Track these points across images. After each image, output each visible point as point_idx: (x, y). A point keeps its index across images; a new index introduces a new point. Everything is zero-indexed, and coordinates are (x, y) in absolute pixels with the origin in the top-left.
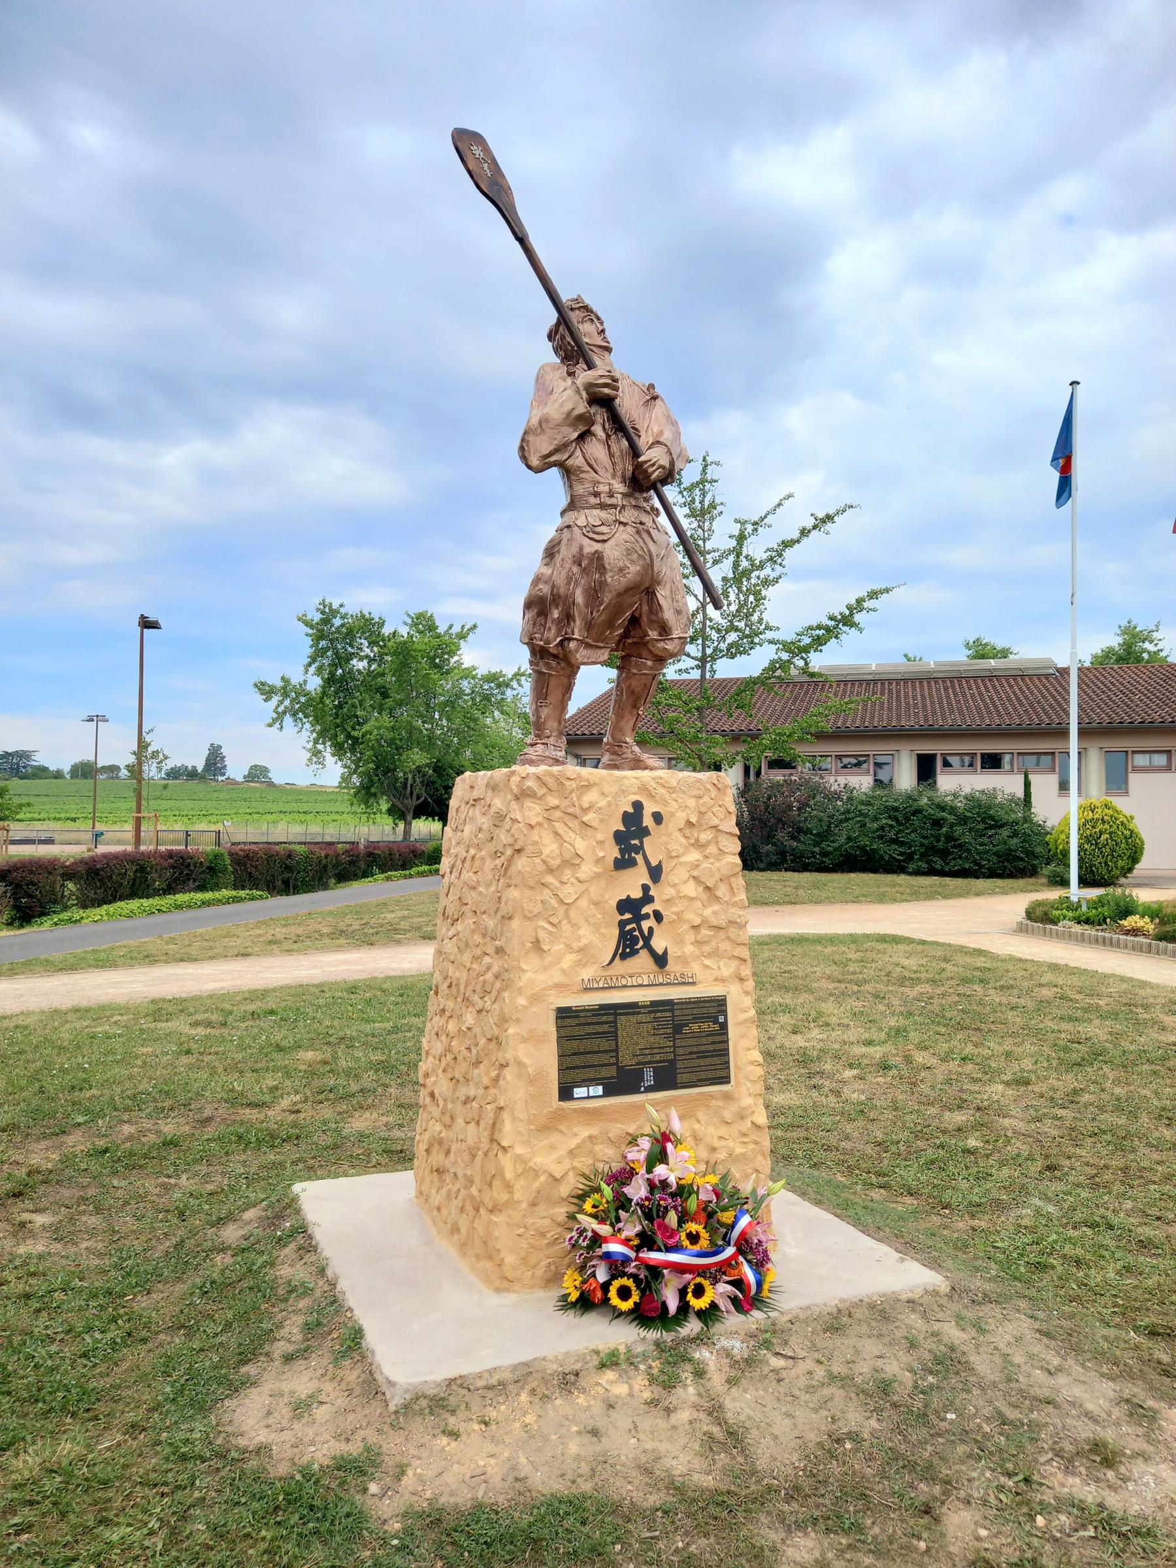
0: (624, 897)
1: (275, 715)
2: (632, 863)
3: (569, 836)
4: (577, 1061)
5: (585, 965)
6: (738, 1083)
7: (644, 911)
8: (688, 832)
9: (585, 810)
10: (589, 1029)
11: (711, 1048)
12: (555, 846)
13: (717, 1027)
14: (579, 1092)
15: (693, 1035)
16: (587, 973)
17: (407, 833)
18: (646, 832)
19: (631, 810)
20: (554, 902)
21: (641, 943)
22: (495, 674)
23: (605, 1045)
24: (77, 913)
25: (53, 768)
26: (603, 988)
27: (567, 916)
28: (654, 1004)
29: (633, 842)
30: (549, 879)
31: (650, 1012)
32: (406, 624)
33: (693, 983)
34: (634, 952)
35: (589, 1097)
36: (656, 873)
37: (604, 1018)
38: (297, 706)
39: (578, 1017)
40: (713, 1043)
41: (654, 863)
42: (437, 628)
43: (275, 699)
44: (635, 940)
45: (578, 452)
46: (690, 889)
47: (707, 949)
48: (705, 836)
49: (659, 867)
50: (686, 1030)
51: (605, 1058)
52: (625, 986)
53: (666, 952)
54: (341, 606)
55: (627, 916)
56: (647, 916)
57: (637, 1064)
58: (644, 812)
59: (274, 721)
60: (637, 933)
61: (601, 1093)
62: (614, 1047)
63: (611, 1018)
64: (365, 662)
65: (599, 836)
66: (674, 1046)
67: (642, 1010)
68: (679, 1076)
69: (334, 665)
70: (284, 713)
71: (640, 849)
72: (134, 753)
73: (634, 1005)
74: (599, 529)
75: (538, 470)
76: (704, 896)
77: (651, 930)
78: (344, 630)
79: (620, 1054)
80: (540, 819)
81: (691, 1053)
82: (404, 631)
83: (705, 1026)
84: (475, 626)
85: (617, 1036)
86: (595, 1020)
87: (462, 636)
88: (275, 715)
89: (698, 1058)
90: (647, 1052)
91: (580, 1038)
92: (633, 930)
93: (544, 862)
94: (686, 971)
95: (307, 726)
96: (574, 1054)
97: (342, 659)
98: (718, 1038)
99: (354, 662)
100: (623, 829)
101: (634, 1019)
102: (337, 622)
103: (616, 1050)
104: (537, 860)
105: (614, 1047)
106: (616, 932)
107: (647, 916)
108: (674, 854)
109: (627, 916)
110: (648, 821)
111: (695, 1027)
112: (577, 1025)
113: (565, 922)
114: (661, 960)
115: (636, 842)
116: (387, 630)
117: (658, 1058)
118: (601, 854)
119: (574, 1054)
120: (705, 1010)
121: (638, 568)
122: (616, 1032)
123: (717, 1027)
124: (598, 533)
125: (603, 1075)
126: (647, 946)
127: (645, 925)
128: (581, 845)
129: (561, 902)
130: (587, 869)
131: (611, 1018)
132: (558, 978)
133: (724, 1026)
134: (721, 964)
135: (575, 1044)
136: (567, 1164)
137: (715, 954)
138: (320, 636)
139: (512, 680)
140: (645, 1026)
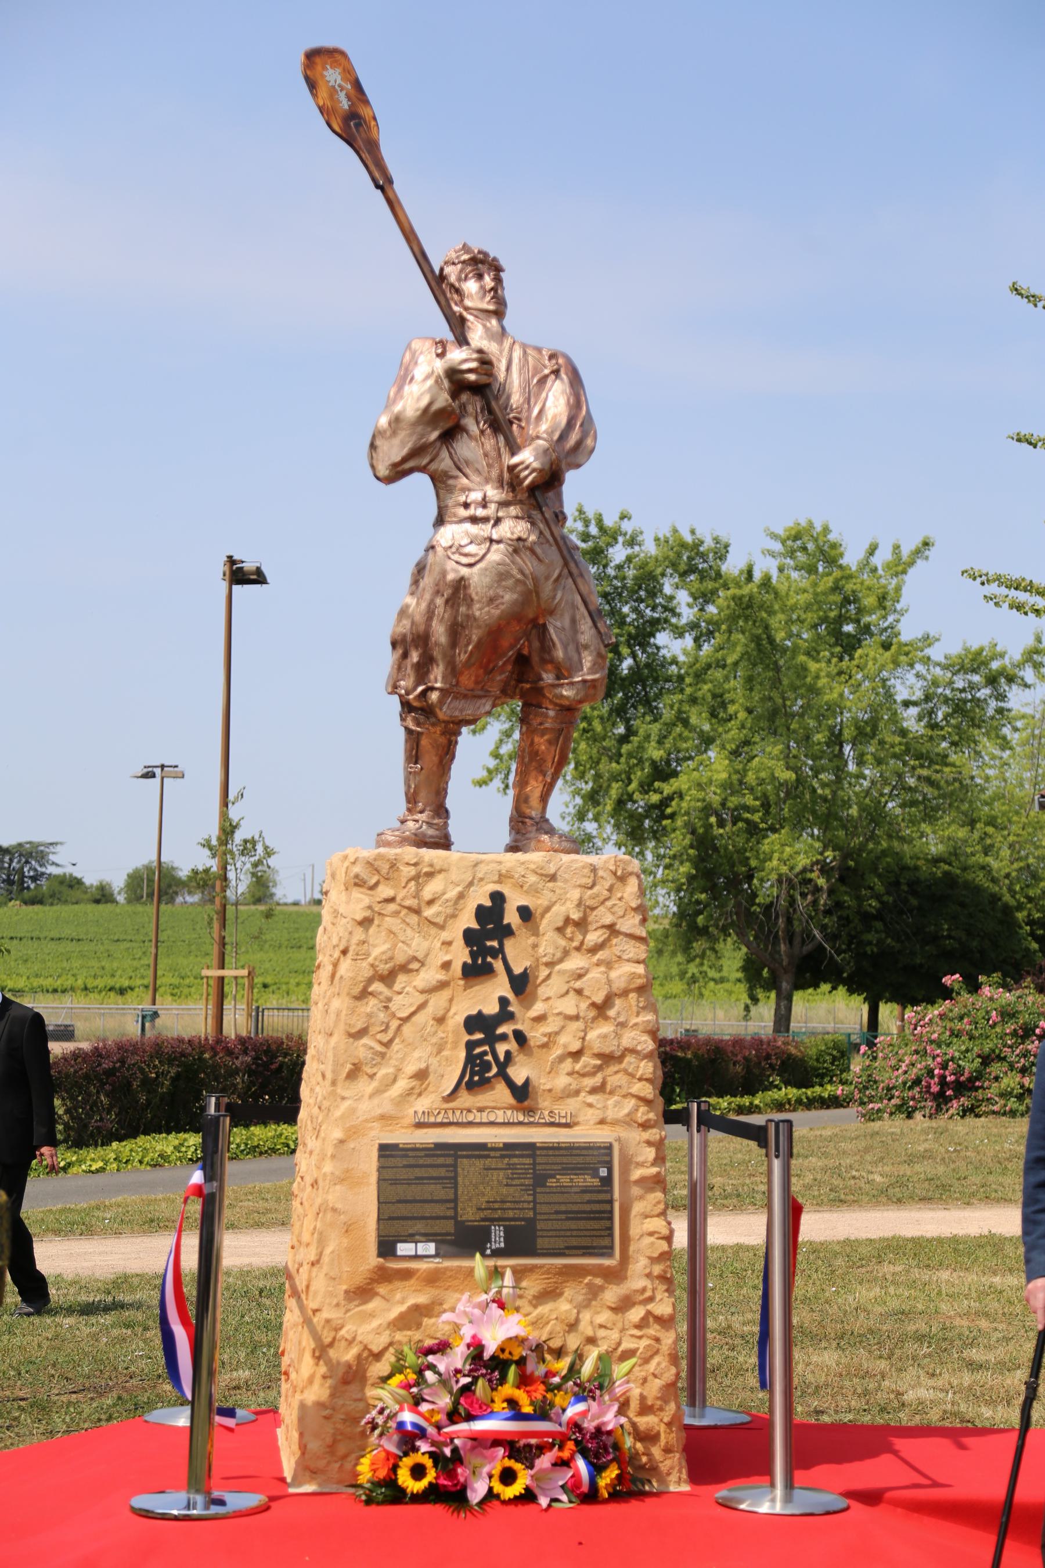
0: (474, 1012)
1: (492, 763)
2: (487, 971)
4: (403, 1210)
7: (500, 1031)
10: (419, 1172)
11: (587, 1207)
13: (596, 1182)
14: (404, 1249)
15: (563, 1190)
17: (783, 1020)
18: (508, 931)
19: (488, 903)
22: (979, 653)
23: (439, 1192)
24: (64, 1156)
25: (91, 879)
28: (508, 1146)
29: (489, 943)
31: (503, 1157)
32: (772, 554)
36: (521, 983)
37: (440, 1161)
39: (407, 1156)
40: (589, 1202)
41: (517, 970)
44: (487, 1067)
45: (444, 454)
50: (551, 1182)
51: (439, 1210)
54: (623, 517)
55: (479, 1036)
56: (504, 1037)
57: (483, 1220)
58: (507, 906)
60: (489, 1058)
62: (452, 1196)
63: (450, 1161)
64: (688, 641)
66: (534, 1202)
67: (492, 1154)
68: (539, 1241)
71: (499, 952)
72: (207, 844)
73: (482, 1146)
74: (466, 550)
75: (389, 480)
78: (631, 573)
79: (460, 1205)
81: (557, 1212)
82: (765, 566)
84: (926, 544)
85: (456, 1184)
86: (429, 1161)
87: (900, 566)
88: (492, 763)
89: (568, 1219)
90: (496, 1206)
91: (409, 1182)
92: (485, 1053)
93: (372, 965)
96: (399, 1202)
99: (662, 638)
101: (479, 1163)
103: (455, 1201)
105: (452, 1196)
106: (462, 1054)
107: (504, 1037)
109: (479, 1036)
110: (511, 917)
111: (565, 1180)
114: (522, 1093)
115: (495, 944)
116: (732, 566)
117: (511, 1214)
119: (399, 1202)
120: (580, 1160)
121: (515, 596)
122: (455, 1178)
124: (466, 555)
125: (437, 1229)
126: (502, 1074)
127: (501, 1049)
131: (450, 1161)
135: (400, 1189)
139: (1020, 666)
140: (495, 1173)
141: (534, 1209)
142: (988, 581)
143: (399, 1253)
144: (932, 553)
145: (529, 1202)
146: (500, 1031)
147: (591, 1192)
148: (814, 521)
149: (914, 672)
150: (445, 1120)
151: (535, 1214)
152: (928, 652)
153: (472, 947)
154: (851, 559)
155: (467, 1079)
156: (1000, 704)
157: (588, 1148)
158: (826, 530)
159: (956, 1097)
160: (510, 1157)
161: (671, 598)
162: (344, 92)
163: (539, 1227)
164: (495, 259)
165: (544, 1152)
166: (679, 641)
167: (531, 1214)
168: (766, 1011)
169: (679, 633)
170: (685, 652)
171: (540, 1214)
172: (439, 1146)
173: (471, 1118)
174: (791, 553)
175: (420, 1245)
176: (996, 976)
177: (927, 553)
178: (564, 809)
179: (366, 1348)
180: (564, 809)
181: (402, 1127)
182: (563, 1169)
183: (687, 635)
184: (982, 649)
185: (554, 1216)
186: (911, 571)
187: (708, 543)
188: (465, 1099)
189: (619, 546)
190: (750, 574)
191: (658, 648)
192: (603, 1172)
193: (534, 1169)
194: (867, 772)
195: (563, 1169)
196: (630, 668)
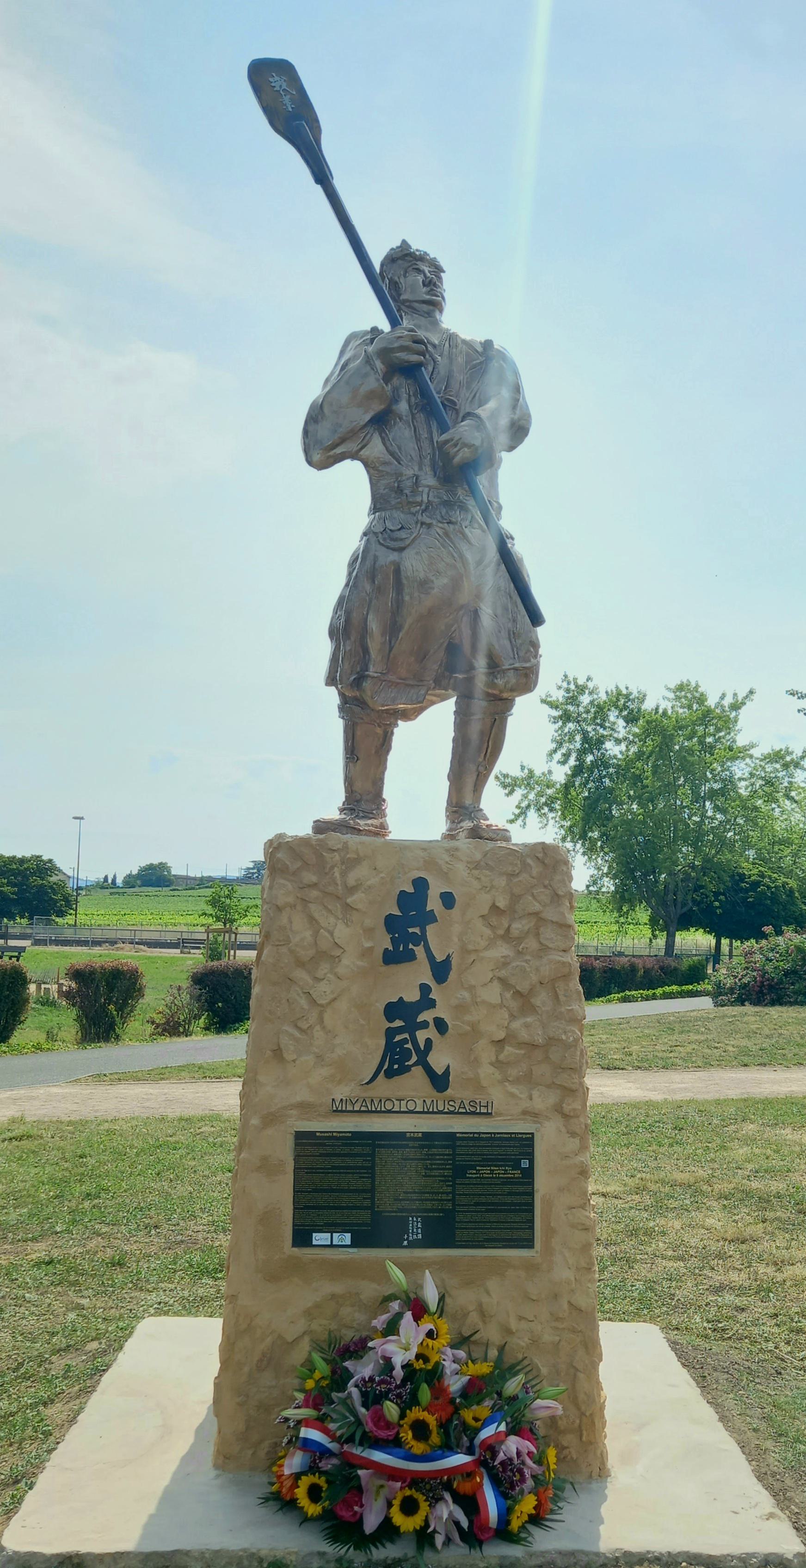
1: (517, 811)
2: (410, 957)
3: (326, 920)
5: (340, 1082)
6: (548, 1250)
7: (420, 1018)
8: (494, 921)
9: (352, 890)
10: (337, 1162)
11: (508, 1199)
12: (308, 934)
13: (517, 1173)
14: (320, 1238)
16: (341, 1092)
18: (431, 918)
19: (411, 890)
20: (303, 1002)
21: (414, 1058)
26: (360, 1111)
27: (321, 1020)
28: (427, 1136)
29: (411, 930)
30: (301, 975)
32: (669, 700)
33: (488, 1114)
34: (404, 1070)
35: (332, 1246)
37: (358, 1150)
38: (543, 800)
40: (510, 1194)
41: (439, 957)
42: (706, 700)
43: (519, 793)
44: (407, 1055)
46: (493, 994)
47: (513, 1072)
48: (518, 927)
49: (447, 961)
50: (471, 1174)
52: (389, 1112)
53: (447, 1071)
55: (398, 1023)
56: (425, 1025)
59: (517, 817)
60: (409, 1046)
61: (348, 1242)
63: (367, 1150)
64: (623, 747)
65: (368, 922)
66: (453, 1193)
69: (582, 752)
70: (528, 807)
71: (421, 939)
76: (514, 1005)
77: (429, 1042)
80: (290, 899)
82: (665, 705)
83: (499, 1171)
84: (751, 692)
86: (346, 1150)
87: (736, 706)
89: (487, 1211)
92: (405, 1041)
93: (292, 952)
94: (478, 1098)
95: (551, 822)
96: (315, 1191)
97: (592, 744)
98: (521, 1189)
100: (397, 913)
102: (585, 699)
103: (372, 1190)
104: (284, 950)
107: (425, 1025)
108: (471, 947)
109: (398, 1023)
110: (434, 904)
111: (485, 1171)
112: (321, 1155)
113: (318, 1028)
114: (440, 1081)
115: (417, 930)
118: (368, 945)
122: (373, 1168)
123: (517, 1173)
124: (395, 540)
126: (423, 1062)
127: (421, 1036)
128: (342, 932)
129: (313, 1002)
130: (349, 962)
131: (367, 1150)
132: (302, 1095)
133: (529, 1174)
134: (535, 1093)
136: (301, 1325)
137: (528, 1079)
138: (566, 717)
141: (453, 1200)
142: (802, 696)
143: (315, 1242)
144: (754, 697)
145: (447, 1193)
146: (420, 1018)
147: (512, 1183)
148: (691, 681)
149: (745, 762)
150: (363, 1109)
151: (454, 1205)
152: (752, 752)
153: (393, 934)
154: (711, 702)
155: (386, 1067)
156: (790, 779)
157: (513, 1138)
158: (697, 686)
159: (769, 994)
160: (429, 1147)
161: (614, 723)
162: (288, 97)
163: (457, 1219)
164: (434, 260)
165: (464, 1143)
166: (618, 747)
167: (449, 1206)
168: (661, 941)
169: (618, 741)
170: (621, 752)
171: (459, 1205)
172: (357, 1135)
173: (389, 1106)
174: (678, 698)
175: (335, 1235)
176: (793, 927)
177: (752, 697)
178: (555, 836)
179: (280, 1337)
180: (555, 836)
181: (319, 1115)
182: (484, 1160)
183: (622, 744)
184: (781, 750)
185: (472, 1208)
186: (744, 708)
187: (635, 694)
188: (384, 1087)
189: (586, 696)
190: (657, 709)
191: (606, 751)
192: (525, 1164)
193: (454, 1160)
194: (718, 816)
195: (484, 1160)
196: (591, 761)
